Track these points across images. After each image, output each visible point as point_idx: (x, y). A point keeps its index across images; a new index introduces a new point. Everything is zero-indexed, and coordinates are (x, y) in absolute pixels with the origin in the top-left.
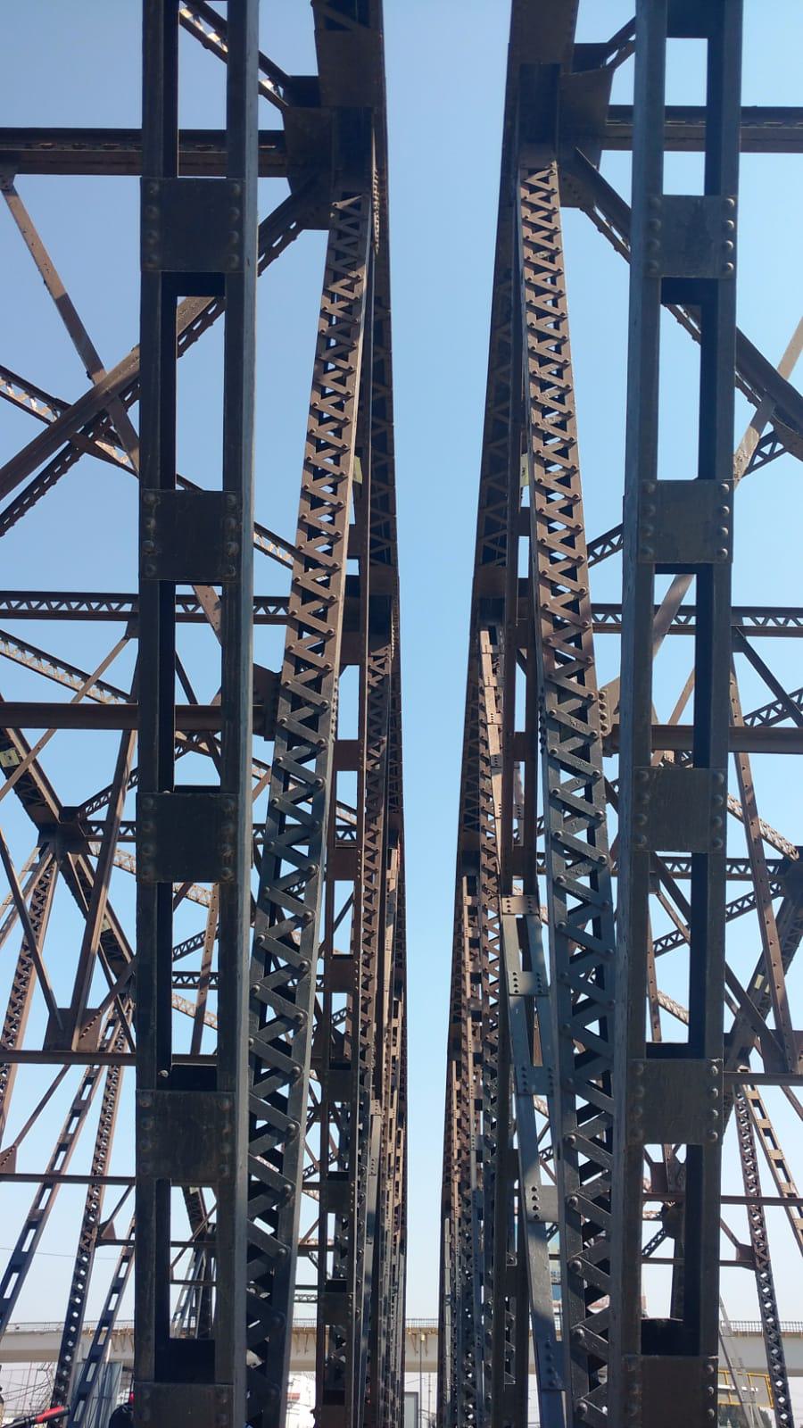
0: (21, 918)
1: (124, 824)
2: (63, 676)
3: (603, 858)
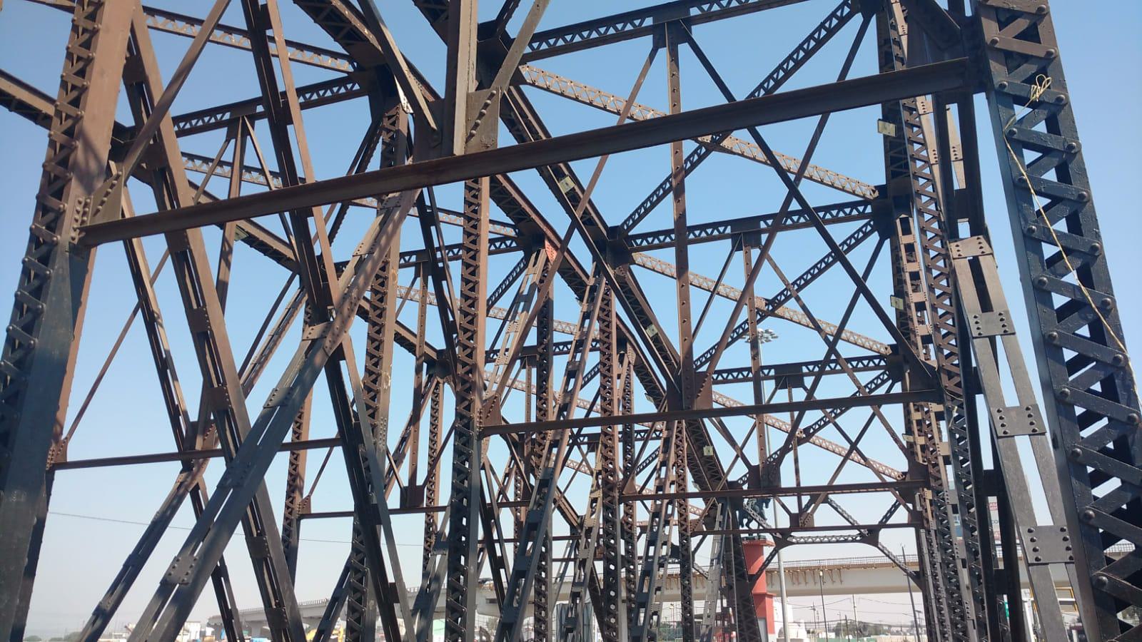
0: (642, 381)
1: (771, 378)
2: (312, 58)
3: (1082, 195)
